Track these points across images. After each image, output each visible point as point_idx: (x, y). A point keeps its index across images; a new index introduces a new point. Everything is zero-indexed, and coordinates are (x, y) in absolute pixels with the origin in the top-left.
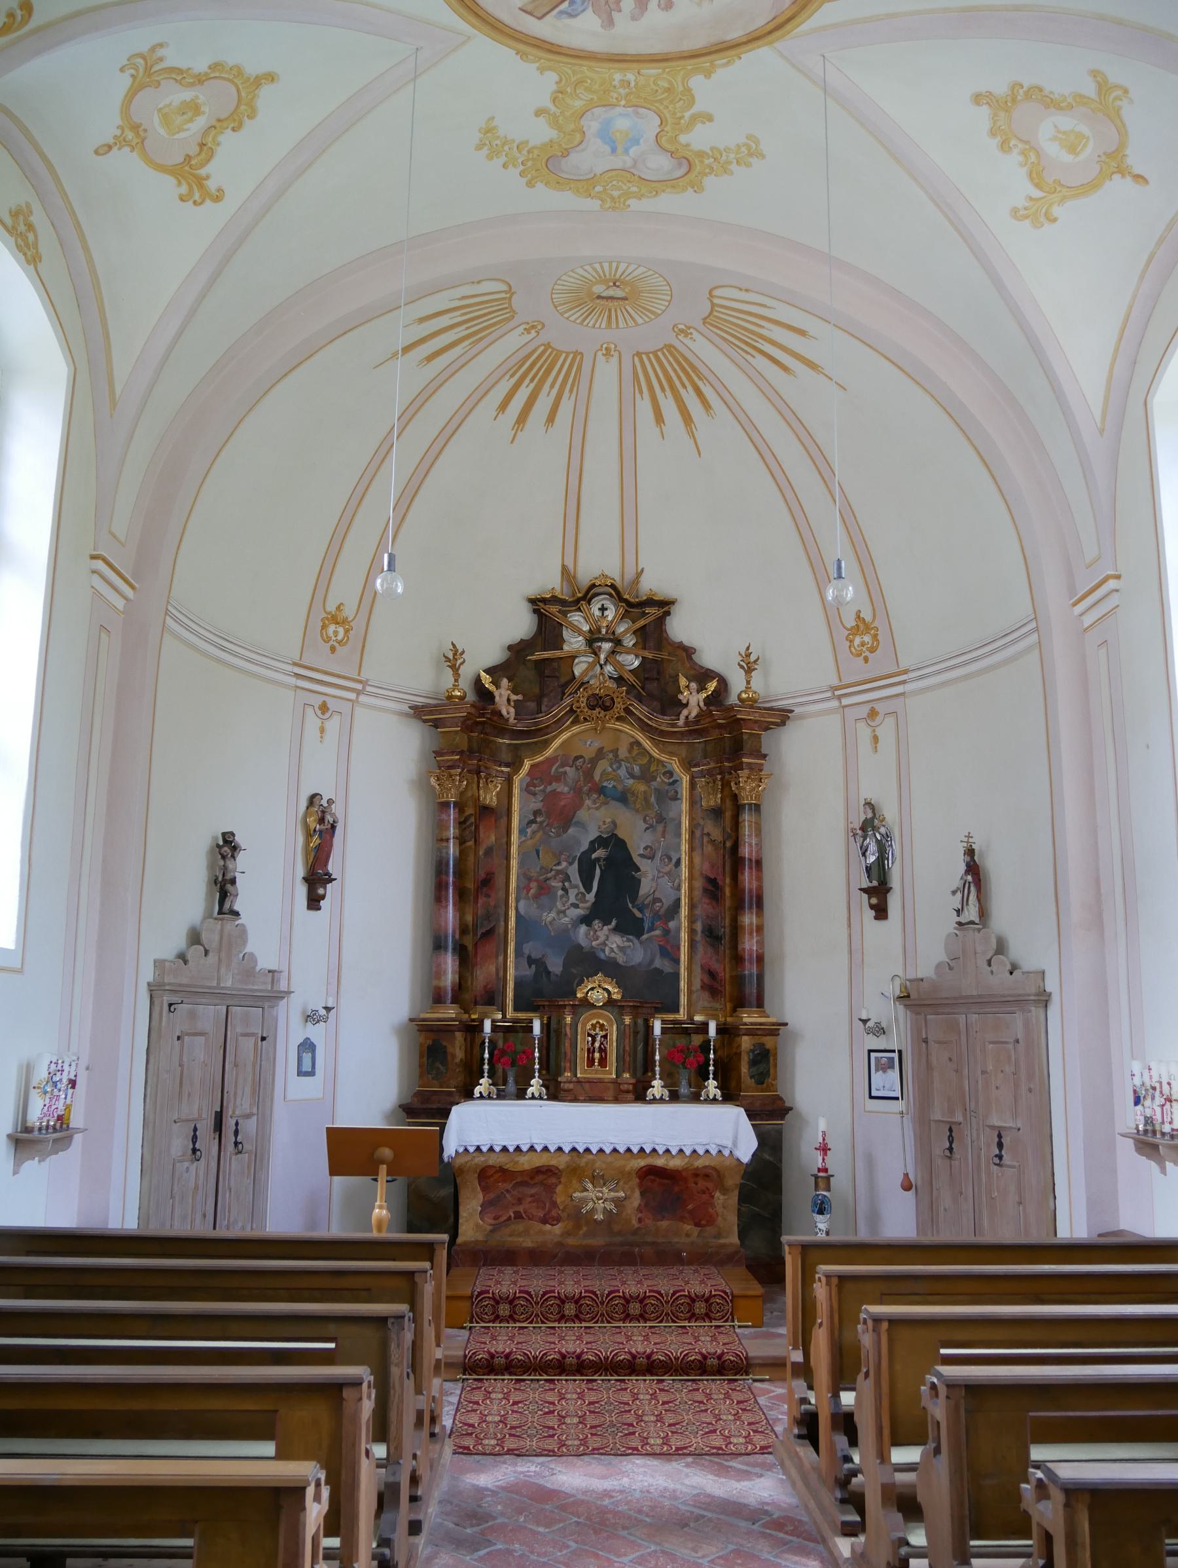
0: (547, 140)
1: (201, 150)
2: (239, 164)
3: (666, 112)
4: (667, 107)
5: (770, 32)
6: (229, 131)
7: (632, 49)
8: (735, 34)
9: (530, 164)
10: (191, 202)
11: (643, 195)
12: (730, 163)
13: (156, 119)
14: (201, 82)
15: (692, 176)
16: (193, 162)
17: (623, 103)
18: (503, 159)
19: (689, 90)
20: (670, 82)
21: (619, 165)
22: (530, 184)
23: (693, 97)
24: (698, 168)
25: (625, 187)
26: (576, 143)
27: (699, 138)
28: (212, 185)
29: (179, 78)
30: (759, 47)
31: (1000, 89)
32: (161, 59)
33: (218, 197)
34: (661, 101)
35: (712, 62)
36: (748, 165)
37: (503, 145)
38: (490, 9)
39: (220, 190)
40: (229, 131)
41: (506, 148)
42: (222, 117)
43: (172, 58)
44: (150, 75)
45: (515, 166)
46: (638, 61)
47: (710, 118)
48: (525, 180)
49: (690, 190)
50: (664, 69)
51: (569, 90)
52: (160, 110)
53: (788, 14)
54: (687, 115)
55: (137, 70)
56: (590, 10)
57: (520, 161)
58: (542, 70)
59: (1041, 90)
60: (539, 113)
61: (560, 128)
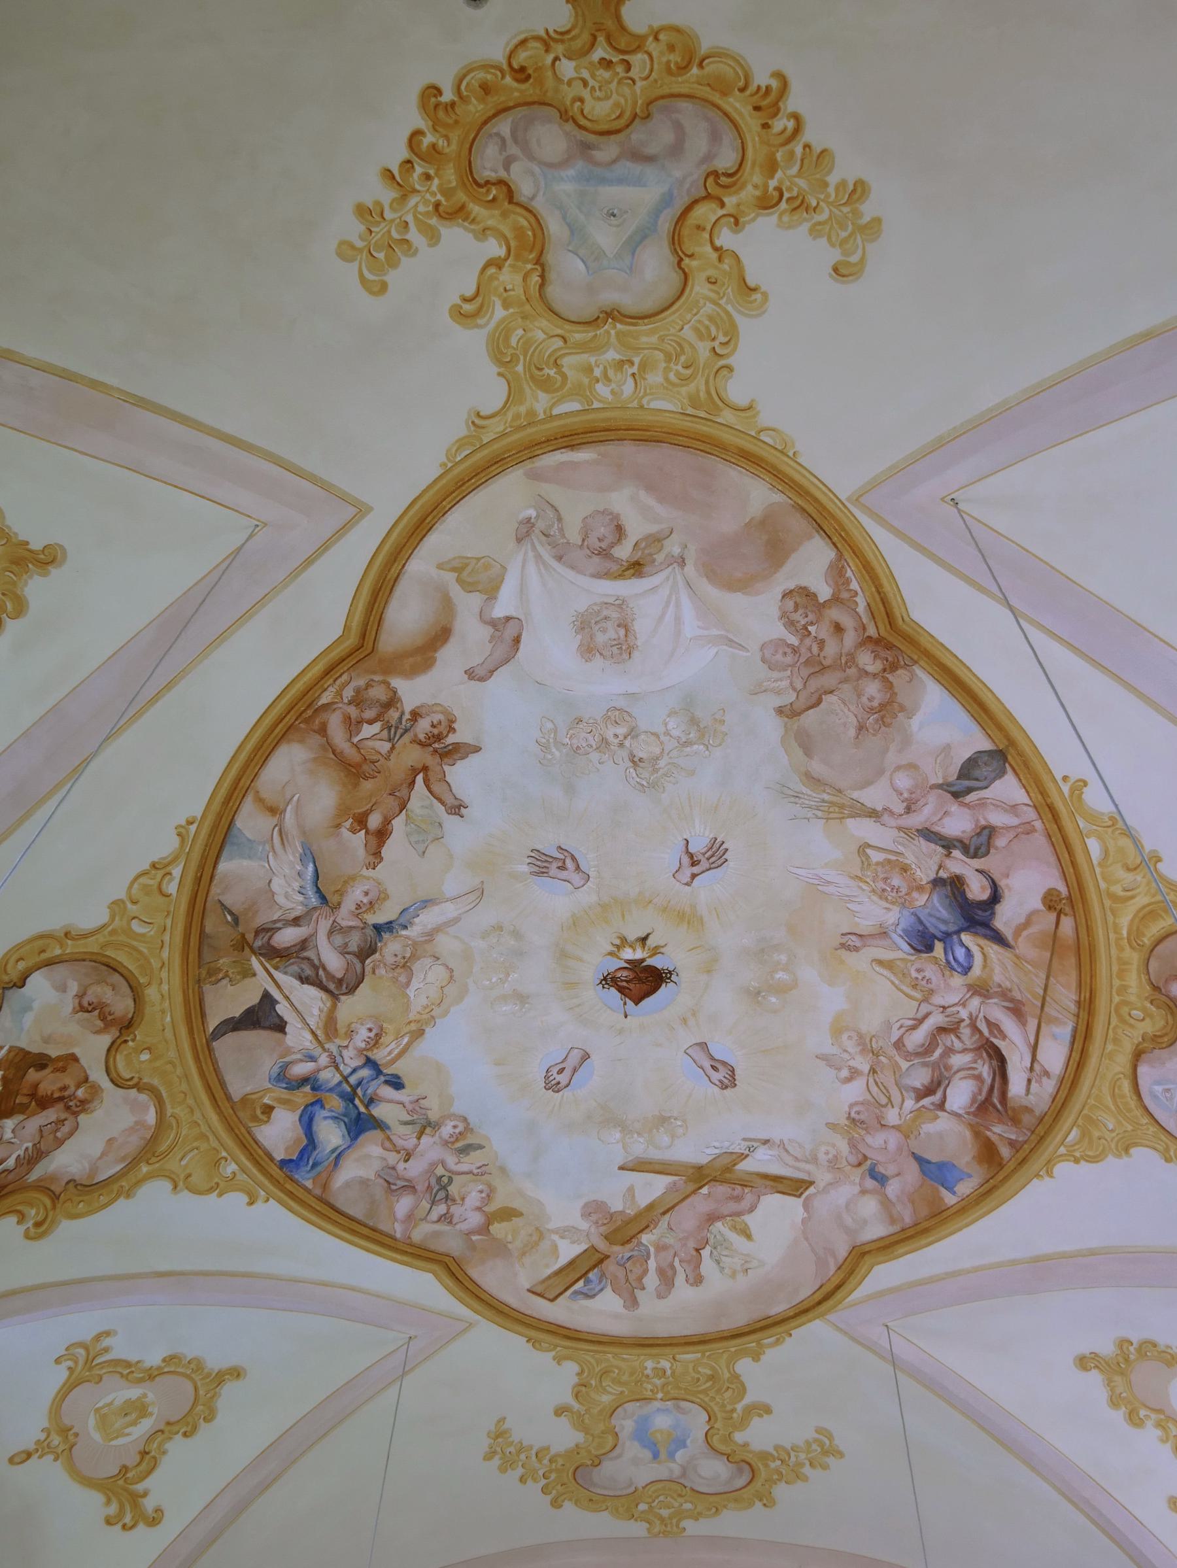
0: (572, 1445)
1: (142, 1459)
2: (186, 1482)
3: (712, 1404)
4: (713, 1399)
5: (819, 1303)
6: (179, 1437)
7: (663, 1330)
8: (779, 1308)
9: (553, 1476)
10: (119, 1526)
11: (700, 1514)
12: (802, 1465)
13: (92, 1422)
14: (151, 1378)
15: (757, 1485)
16: (129, 1475)
17: (660, 1395)
18: (520, 1471)
19: (736, 1377)
20: (712, 1368)
21: (665, 1475)
22: (556, 1504)
23: (743, 1384)
24: (763, 1474)
25: (676, 1504)
26: (608, 1448)
27: (758, 1436)
28: (149, 1504)
29: (125, 1372)
30: (810, 1321)
31: (1106, 1348)
32: (106, 1350)
33: (154, 1520)
34: (705, 1392)
35: (758, 1342)
36: (825, 1467)
37: (519, 1452)
38: (494, 1292)
39: (158, 1510)
40: (179, 1437)
41: (523, 1457)
42: (172, 1420)
43: (120, 1348)
44: (90, 1369)
45: (535, 1480)
46: (670, 1345)
47: (767, 1410)
48: (549, 1498)
49: (758, 1504)
50: (703, 1353)
51: (593, 1382)
52: (97, 1410)
53: (836, 1281)
54: (739, 1407)
55: (76, 1363)
56: (609, 1289)
57: (541, 1473)
58: (559, 1360)
59: (1155, 1345)
60: (560, 1411)
61: (586, 1430)
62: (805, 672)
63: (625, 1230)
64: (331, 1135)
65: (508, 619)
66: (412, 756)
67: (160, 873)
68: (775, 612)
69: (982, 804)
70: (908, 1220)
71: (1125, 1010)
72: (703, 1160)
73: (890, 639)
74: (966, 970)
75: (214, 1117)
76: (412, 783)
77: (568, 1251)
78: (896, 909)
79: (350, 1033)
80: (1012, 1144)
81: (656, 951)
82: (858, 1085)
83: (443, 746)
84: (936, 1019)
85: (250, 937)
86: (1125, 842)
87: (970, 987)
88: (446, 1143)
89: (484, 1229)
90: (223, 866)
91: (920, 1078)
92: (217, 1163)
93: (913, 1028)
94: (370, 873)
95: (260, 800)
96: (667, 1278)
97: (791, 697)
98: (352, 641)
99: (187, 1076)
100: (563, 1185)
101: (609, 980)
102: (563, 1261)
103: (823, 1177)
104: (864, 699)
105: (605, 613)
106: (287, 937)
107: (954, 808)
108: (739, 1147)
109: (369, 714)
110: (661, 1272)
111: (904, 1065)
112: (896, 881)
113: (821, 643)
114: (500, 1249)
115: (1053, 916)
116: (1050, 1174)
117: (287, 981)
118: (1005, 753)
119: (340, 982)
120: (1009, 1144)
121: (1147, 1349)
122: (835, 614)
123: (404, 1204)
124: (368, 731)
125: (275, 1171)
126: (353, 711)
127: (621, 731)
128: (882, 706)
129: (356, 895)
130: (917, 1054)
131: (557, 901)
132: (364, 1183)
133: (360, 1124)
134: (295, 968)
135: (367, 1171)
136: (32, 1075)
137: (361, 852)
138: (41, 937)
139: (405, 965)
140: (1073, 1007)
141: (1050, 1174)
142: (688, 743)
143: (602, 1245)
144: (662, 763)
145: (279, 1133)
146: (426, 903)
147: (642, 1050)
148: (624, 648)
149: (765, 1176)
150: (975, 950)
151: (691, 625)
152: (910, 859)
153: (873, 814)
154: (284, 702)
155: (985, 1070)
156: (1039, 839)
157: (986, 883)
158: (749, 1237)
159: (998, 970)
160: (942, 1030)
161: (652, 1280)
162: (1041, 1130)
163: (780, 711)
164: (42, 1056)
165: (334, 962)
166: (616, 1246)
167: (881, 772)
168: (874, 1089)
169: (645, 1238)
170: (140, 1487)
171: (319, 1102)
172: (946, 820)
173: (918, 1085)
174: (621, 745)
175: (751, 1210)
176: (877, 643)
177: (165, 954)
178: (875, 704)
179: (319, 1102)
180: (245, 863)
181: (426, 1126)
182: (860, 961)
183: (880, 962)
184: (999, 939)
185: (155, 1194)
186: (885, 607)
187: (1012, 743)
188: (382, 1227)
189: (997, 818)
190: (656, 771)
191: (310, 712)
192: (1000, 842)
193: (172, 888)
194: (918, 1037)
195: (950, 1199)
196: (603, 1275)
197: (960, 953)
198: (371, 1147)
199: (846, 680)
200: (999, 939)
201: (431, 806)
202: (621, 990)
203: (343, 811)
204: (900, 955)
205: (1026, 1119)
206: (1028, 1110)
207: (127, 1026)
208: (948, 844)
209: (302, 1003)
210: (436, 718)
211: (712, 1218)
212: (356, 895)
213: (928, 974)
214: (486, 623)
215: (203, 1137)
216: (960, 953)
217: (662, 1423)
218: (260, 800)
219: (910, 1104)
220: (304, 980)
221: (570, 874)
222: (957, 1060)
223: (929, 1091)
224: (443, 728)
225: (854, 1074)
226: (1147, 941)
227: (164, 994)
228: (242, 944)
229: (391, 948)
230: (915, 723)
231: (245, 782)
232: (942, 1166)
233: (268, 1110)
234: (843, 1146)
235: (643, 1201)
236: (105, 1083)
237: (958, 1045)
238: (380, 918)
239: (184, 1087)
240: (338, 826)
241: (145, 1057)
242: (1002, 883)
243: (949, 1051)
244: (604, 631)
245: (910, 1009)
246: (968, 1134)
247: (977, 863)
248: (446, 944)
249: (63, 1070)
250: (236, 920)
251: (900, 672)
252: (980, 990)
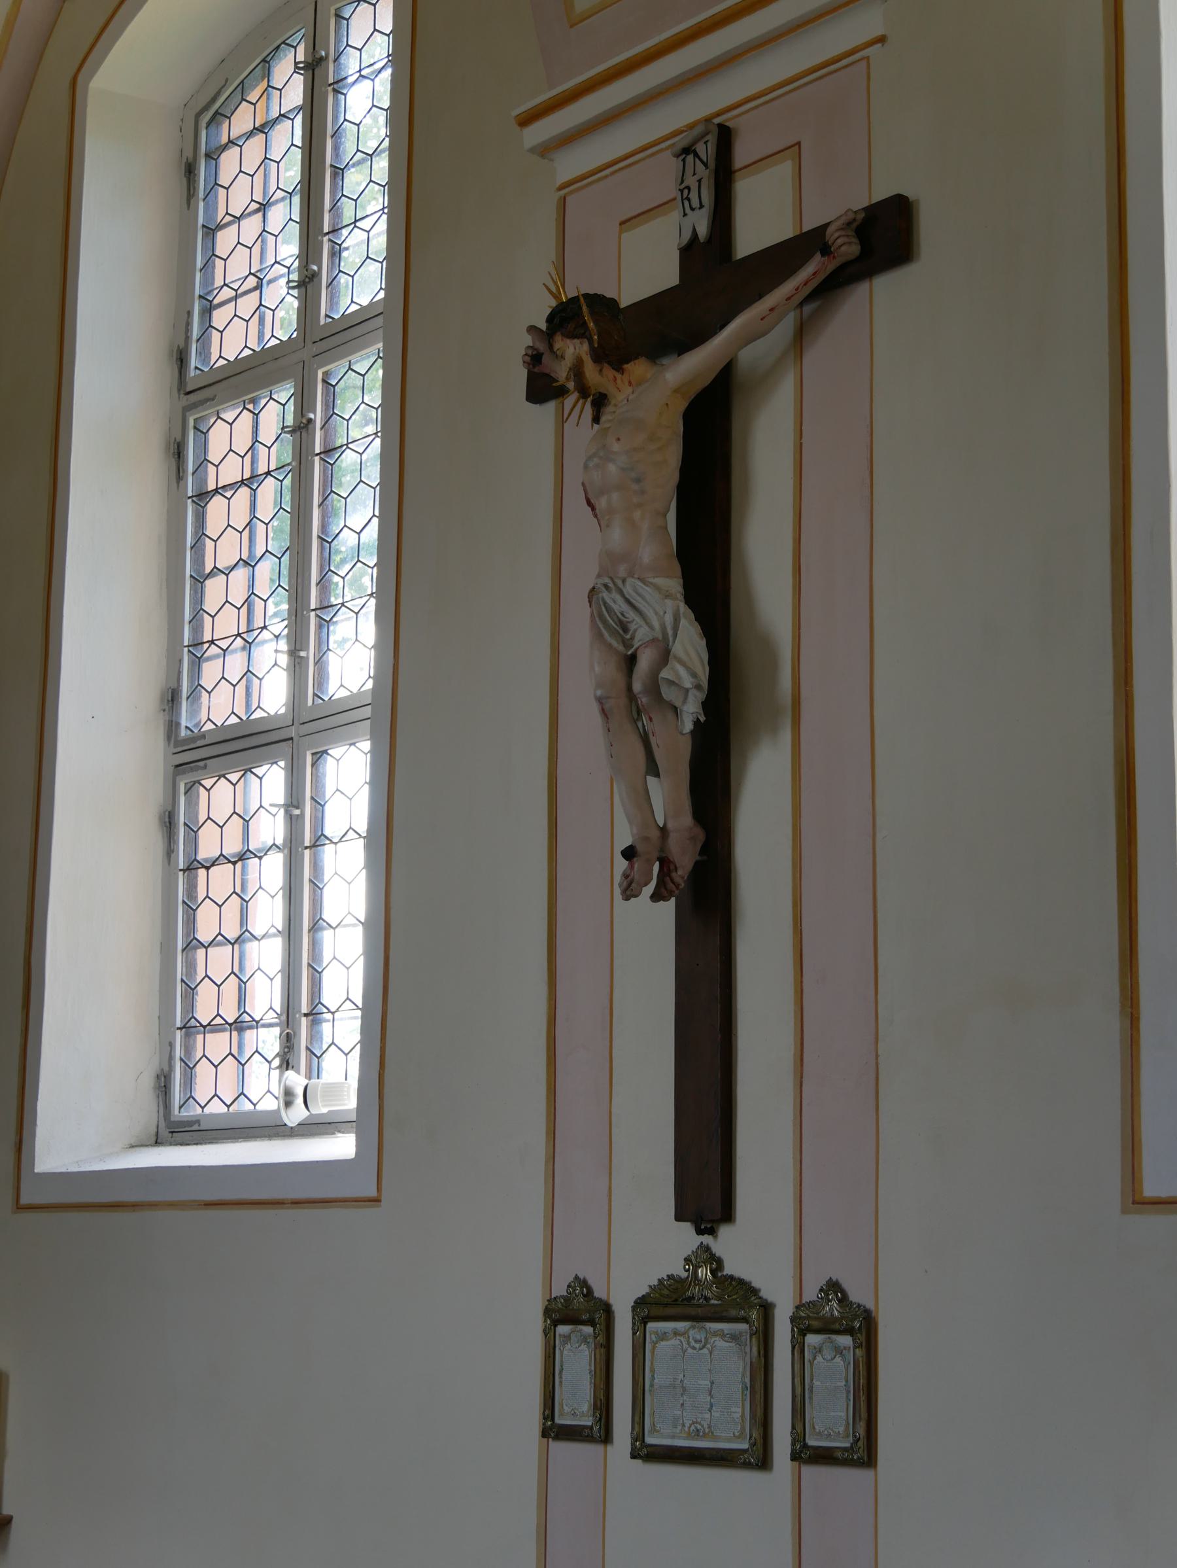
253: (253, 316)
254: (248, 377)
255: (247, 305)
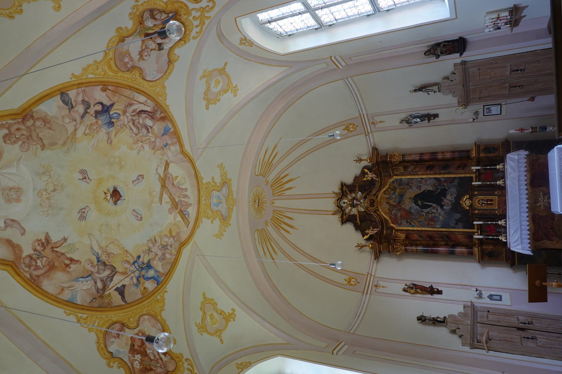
7: (197, 199)
8: (193, 172)
13: (214, 326)
15: (227, 182)
19: (206, 184)
22: (230, 225)
27: (218, 180)
28: (231, 312)
31: (205, 103)
33: (234, 310)
36: (224, 167)
39: (232, 310)
43: (199, 321)
47: (213, 177)
58: (202, 222)
62: (31, 141)
63: (175, 205)
64: (151, 273)
65: (5, 222)
66: (48, 251)
67: (81, 320)
68: (10, 146)
69: (76, 101)
70: (176, 140)
71: (133, 79)
72: (160, 185)
73: (23, 115)
74: (119, 115)
75: (147, 302)
76: (56, 251)
77: (179, 218)
78: (102, 129)
79: (127, 268)
80: (161, 113)
81: (108, 190)
82: (145, 145)
83: (46, 243)
84: (131, 124)
85: (99, 295)
86: (90, 68)
87: (124, 115)
88: (154, 245)
89: (174, 237)
90: (79, 303)
91: (144, 131)
92: (158, 300)
93: (132, 130)
94: (82, 263)
95: (59, 294)
96: (186, 196)
97: (38, 146)
98: (9, 268)
99: (136, 309)
100: (164, 219)
101: (115, 203)
102: (181, 220)
103: (165, 158)
104: (41, 126)
105: (6, 194)
106: (100, 285)
107: (76, 109)
108: (157, 176)
109: (34, 263)
110: (184, 198)
111: (141, 134)
112: (95, 127)
113: (22, 135)
114: (178, 234)
115: (108, 91)
116: (168, 106)
117: (112, 284)
118: (62, 93)
119: (112, 271)
120: (160, 113)
121: (206, 94)
122: (13, 129)
123: (168, 256)
124: (39, 263)
125: (159, 286)
126: (32, 268)
127: (45, 193)
128: (44, 122)
129: (89, 267)
130: (139, 130)
131: (93, 215)
132: (163, 265)
133: (149, 266)
134: (108, 283)
135: (160, 264)
136: (136, 347)
137: (76, 265)
138: (98, 349)
139: (109, 254)
140: (131, 91)
141: (168, 106)
142: (50, 176)
143: (178, 210)
144: (55, 183)
145: (150, 285)
146: (92, 248)
147: (132, 195)
148: (18, 190)
149: (165, 171)
150: (114, 111)
151: (13, 170)
152: (89, 123)
153: (76, 130)
154: (28, 288)
155: (144, 115)
156: (87, 89)
157: (97, 105)
158: (177, 177)
159: (120, 107)
160: (133, 124)
161: (186, 200)
162: (159, 106)
163: (42, 149)
164: (131, 345)
165: (107, 272)
166: (178, 207)
167: (64, 126)
168: (146, 142)
169: (177, 200)
170: (227, 314)
171: (143, 276)
172: (79, 111)
173: (146, 132)
174: (49, 194)
175: (172, 175)
176: (24, 119)
177: (104, 316)
178: (43, 123)
179: (143, 276)
180: (78, 297)
181: (149, 250)
182: (115, 141)
183: (115, 135)
184: (112, 105)
185: (164, 315)
186: (13, 115)
187: (59, 90)
188: (173, 261)
189: (80, 98)
190: (58, 185)
191: (32, 280)
192: (87, 99)
193: (85, 316)
194: (135, 130)
195: (172, 130)
196: (184, 211)
197: (115, 115)
198: (154, 263)
199: (35, 130)
200: (112, 105)
201: (64, 247)
202: (118, 200)
203: (64, 271)
204: (114, 130)
205: (156, 108)
206: (154, 108)
207: (123, 325)
208: (86, 112)
209: (118, 281)
210: (36, 244)
211: (173, 184)
212: (89, 267)
213: (119, 124)
214: (6, 229)
215: (151, 304)
216: (115, 115)
217: (215, 201)
218: (59, 294)
219: (150, 135)
220: (112, 280)
221: (86, 211)
222: (141, 122)
223: (148, 129)
224: (40, 243)
225: (142, 146)
226: (117, 69)
227: (115, 316)
228: (102, 297)
229: (104, 258)
230: (50, 114)
231: (54, 298)
232: (165, 130)
233: (145, 288)
234: (159, 152)
235: (168, 200)
236: (138, 329)
237: (137, 121)
238: (96, 261)
239: (139, 309)
240: (68, 272)
241: (131, 320)
242: (98, 101)
243: (139, 123)
244: (12, 195)
245: (127, 130)
246: (158, 122)
247: (92, 106)
248: (103, 244)
249: (134, 340)
250: (95, 298)
251: (34, 115)
252: (125, 112)
253: (308, 21)
254: (316, 18)
255: (306, 22)
